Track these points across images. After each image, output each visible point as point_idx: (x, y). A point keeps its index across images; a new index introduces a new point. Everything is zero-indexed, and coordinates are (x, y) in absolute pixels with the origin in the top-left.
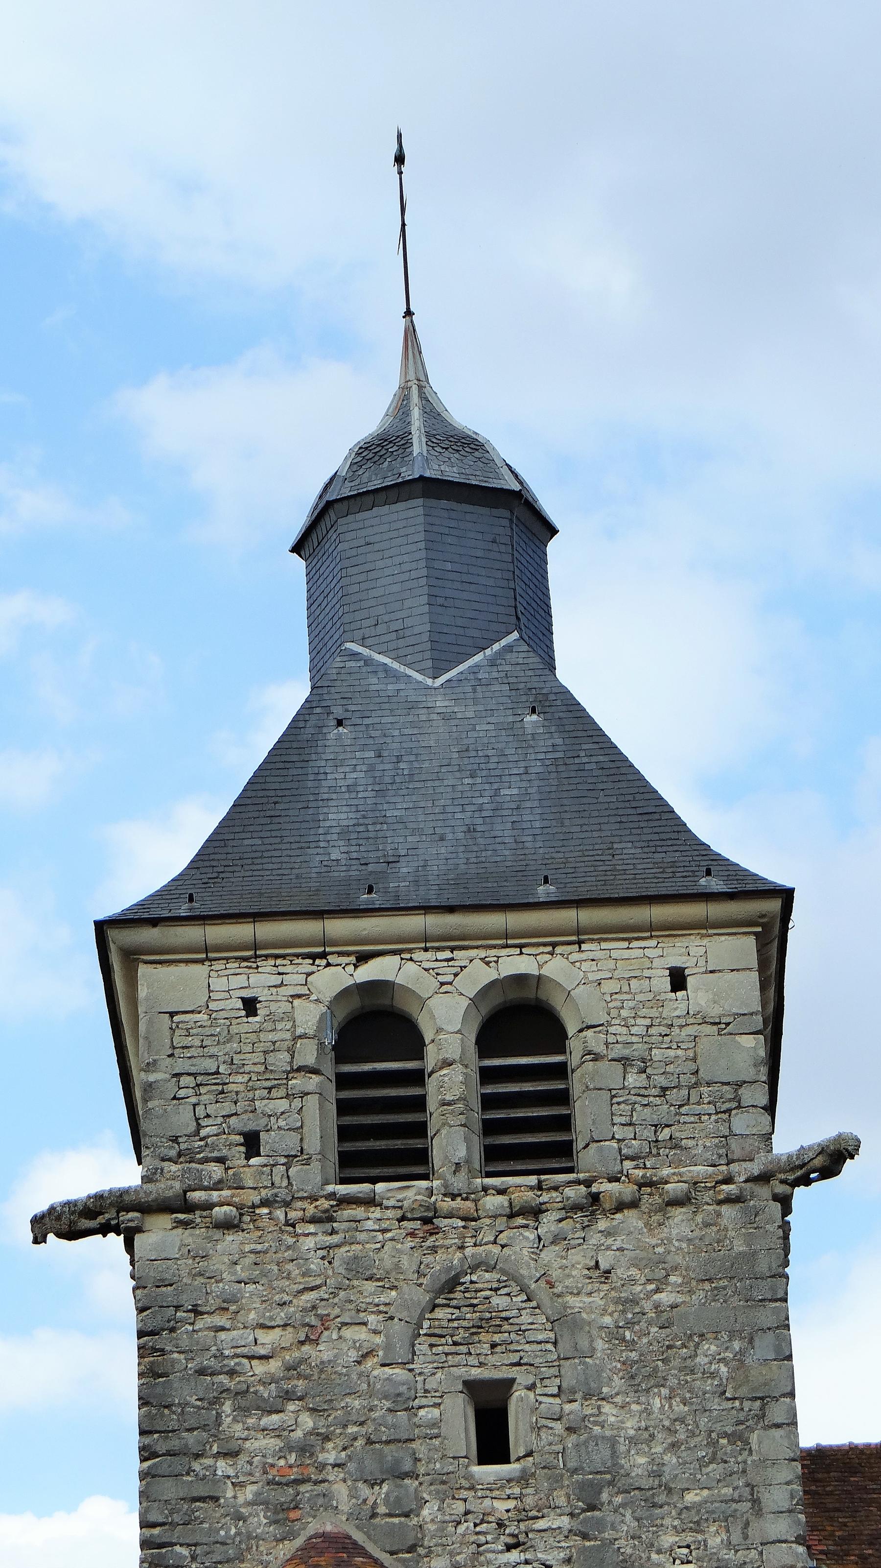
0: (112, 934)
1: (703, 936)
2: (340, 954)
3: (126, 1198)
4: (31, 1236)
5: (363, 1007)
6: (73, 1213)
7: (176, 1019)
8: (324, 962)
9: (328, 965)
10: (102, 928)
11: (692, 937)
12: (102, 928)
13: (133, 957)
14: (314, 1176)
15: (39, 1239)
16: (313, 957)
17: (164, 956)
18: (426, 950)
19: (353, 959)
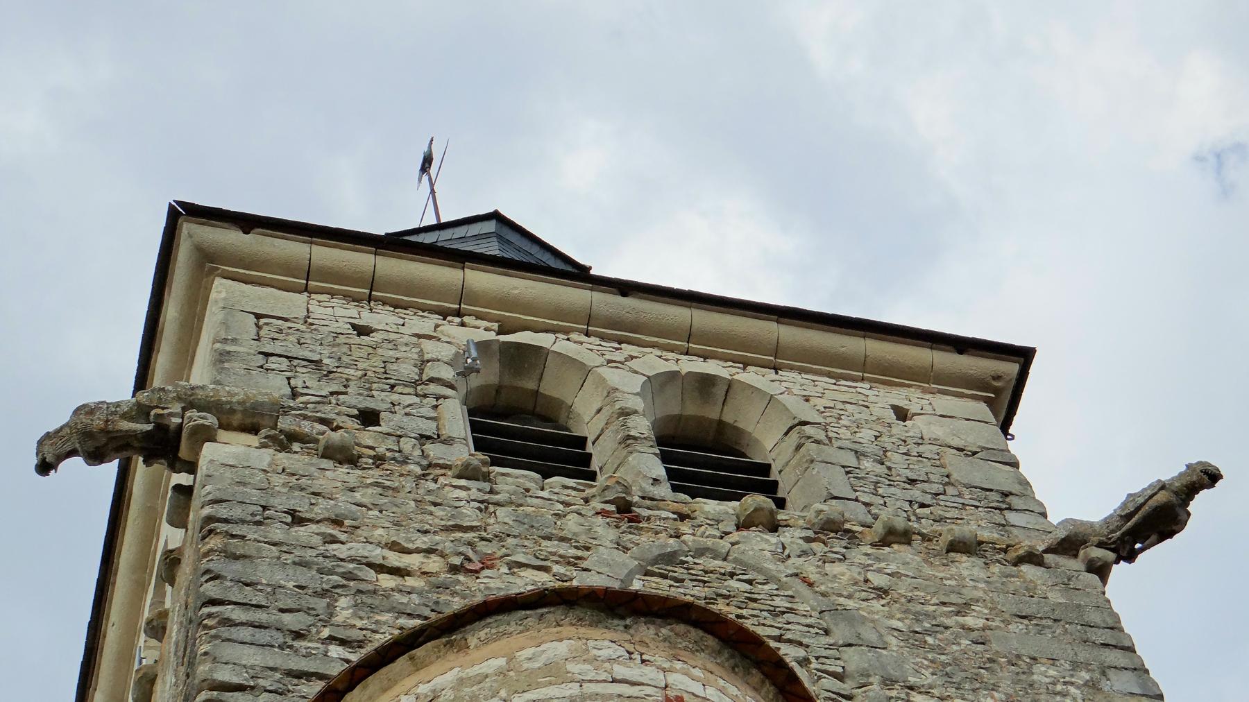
0: (190, 230)
1: (925, 391)
2: (479, 317)
3: (200, 393)
4: (34, 461)
5: (499, 389)
6: (113, 413)
7: (262, 321)
8: (458, 320)
9: (463, 324)
10: (181, 214)
11: (912, 390)
12: (181, 214)
13: (209, 262)
14: (463, 452)
15: (45, 467)
16: (444, 314)
17: (249, 270)
18: (587, 334)
19: (496, 326)
